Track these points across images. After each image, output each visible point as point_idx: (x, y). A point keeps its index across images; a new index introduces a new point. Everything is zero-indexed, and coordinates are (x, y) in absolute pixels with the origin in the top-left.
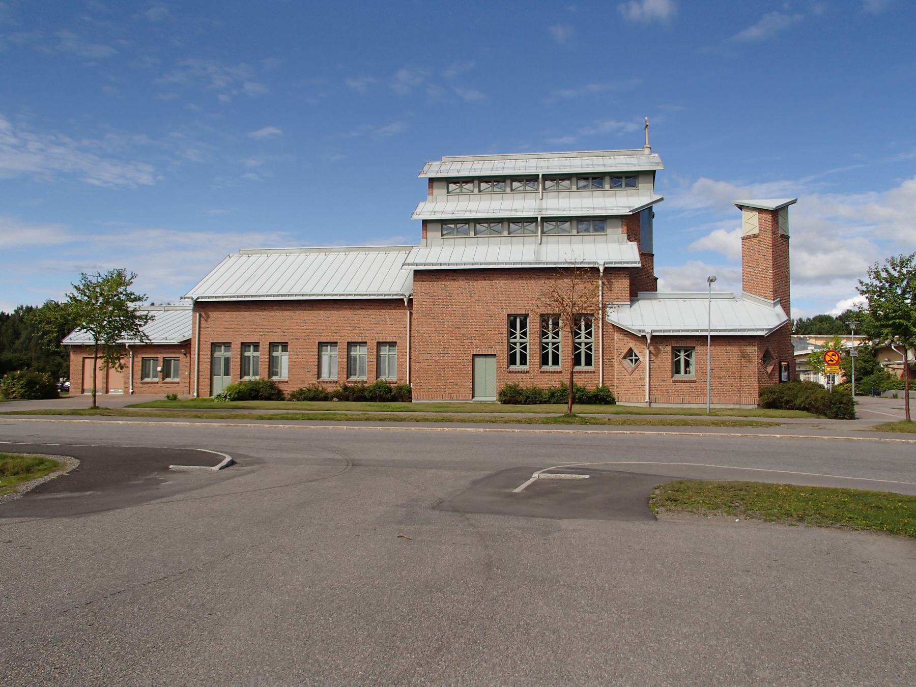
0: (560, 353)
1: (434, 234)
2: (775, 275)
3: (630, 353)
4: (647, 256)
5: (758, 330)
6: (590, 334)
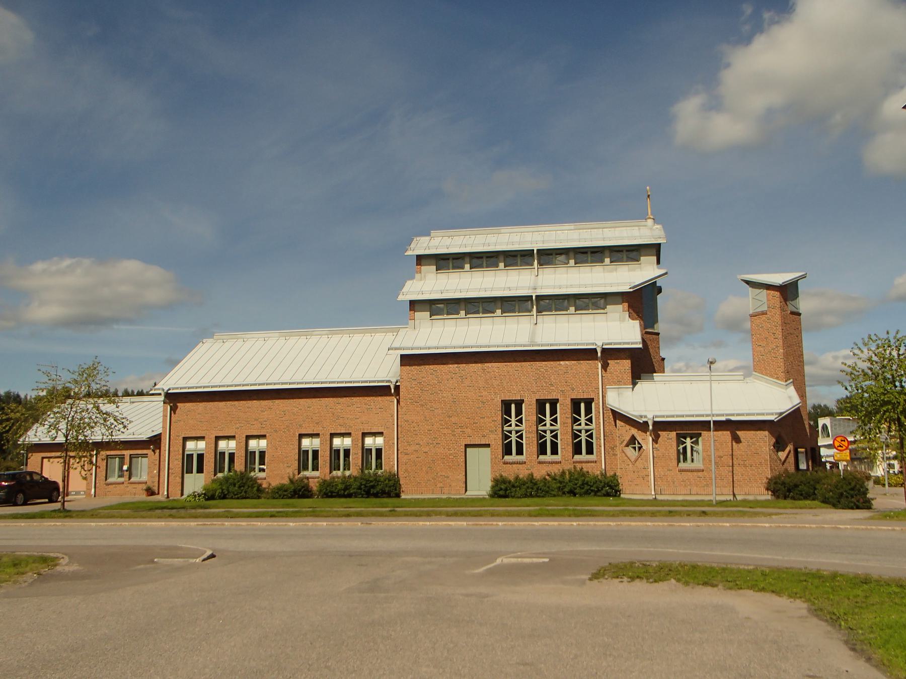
0: (559, 442)
1: (423, 316)
2: (786, 355)
3: (633, 440)
4: (650, 334)
5: (768, 414)
6: (590, 420)
